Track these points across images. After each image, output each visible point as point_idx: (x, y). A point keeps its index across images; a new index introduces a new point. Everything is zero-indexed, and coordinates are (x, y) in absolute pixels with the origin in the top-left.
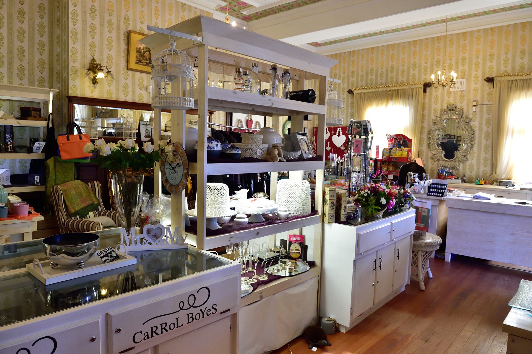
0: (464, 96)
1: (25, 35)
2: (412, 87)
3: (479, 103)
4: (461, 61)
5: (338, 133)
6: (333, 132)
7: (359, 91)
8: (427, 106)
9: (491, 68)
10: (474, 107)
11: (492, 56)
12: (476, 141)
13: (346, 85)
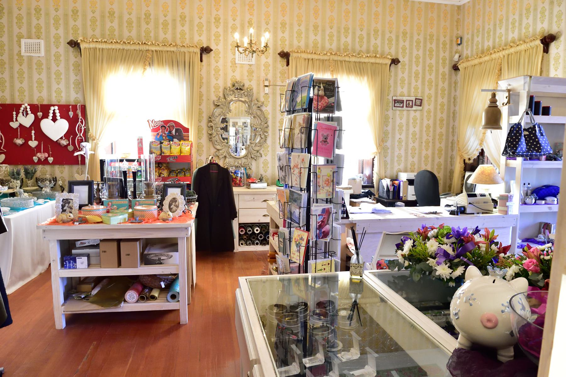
0: (253, 72)
1: (25, 94)
2: (183, 50)
3: (271, 84)
4: (280, 26)
5: (51, 115)
6: (40, 114)
7: (92, 45)
8: (204, 81)
9: (283, 40)
10: (266, 88)
11: (283, 25)
12: (270, 132)
13: (61, 32)
